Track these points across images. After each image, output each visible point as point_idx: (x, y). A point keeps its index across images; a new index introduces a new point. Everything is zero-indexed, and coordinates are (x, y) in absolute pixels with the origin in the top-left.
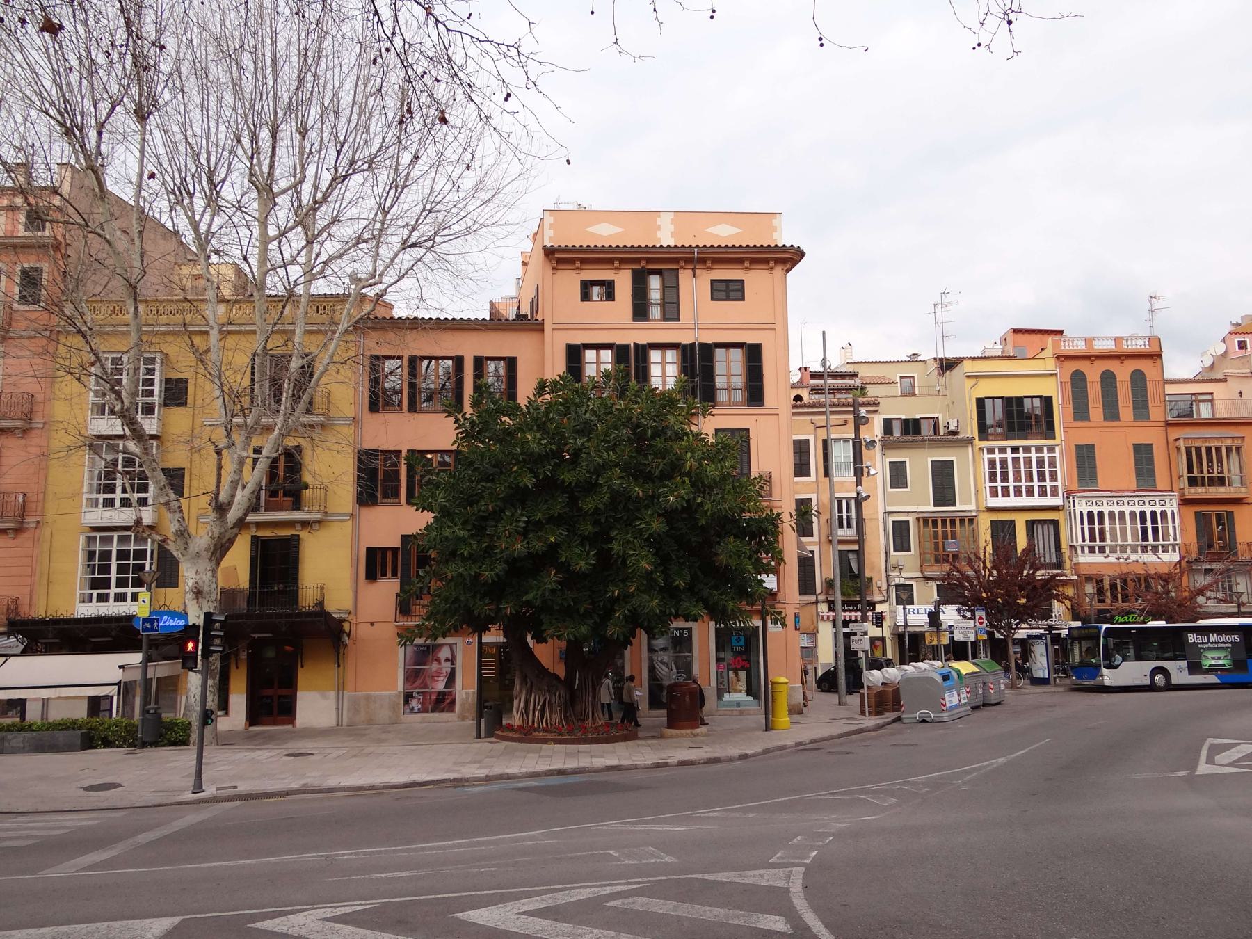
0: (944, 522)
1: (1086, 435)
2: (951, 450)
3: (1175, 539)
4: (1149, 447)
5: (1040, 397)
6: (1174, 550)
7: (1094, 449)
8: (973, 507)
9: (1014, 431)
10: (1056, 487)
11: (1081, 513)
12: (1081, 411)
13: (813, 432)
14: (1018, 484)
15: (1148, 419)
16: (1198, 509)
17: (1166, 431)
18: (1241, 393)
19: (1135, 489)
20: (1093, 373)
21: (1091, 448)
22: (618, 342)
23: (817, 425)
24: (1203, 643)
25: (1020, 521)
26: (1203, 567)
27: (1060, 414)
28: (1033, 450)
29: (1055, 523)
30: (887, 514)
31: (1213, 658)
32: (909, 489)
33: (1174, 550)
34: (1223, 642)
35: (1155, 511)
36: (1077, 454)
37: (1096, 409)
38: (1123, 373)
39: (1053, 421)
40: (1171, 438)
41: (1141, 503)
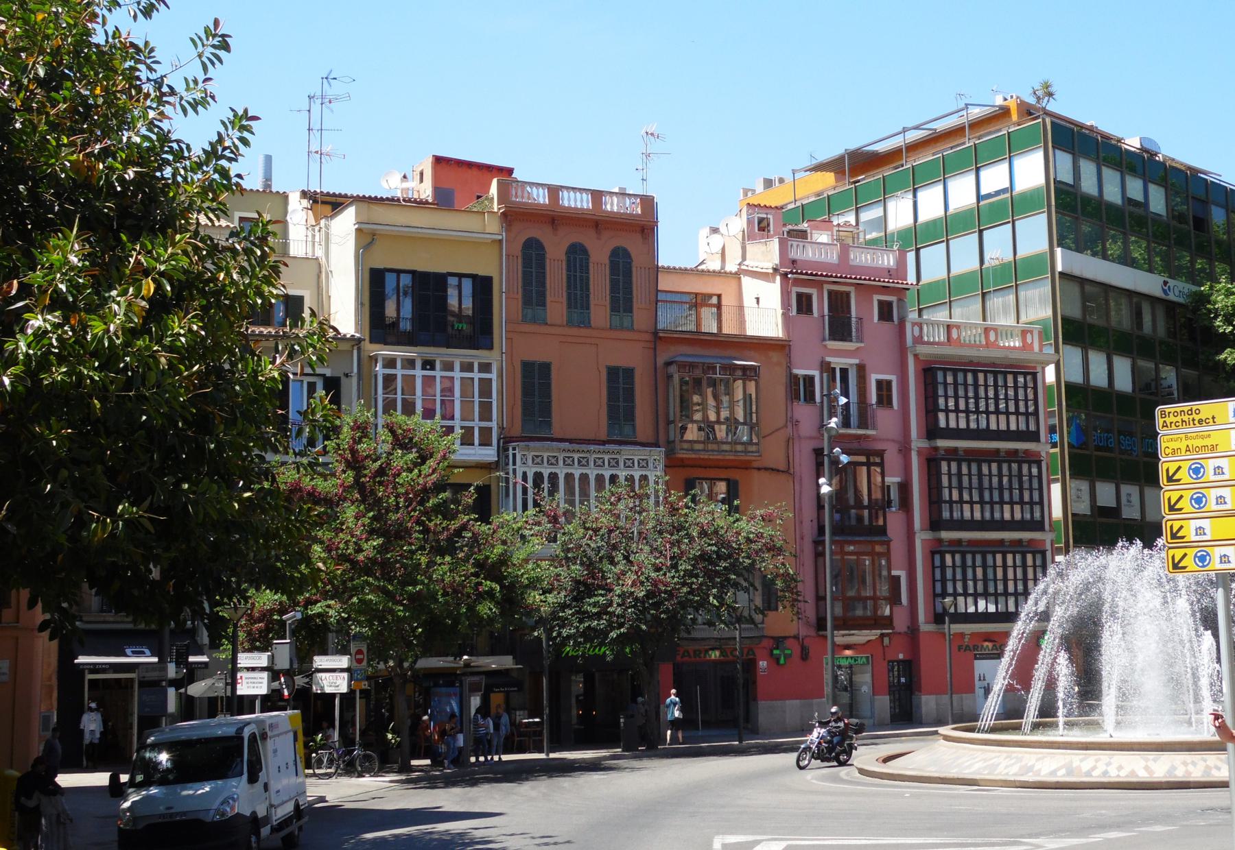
4: (629, 373)
5: (413, 273)
11: (525, 474)
14: (485, 424)
17: (655, 349)
18: (758, 299)
21: (545, 368)
22: (481, 273)
27: (503, 307)
35: (602, 475)
37: (556, 304)
38: (599, 254)
39: (491, 319)
40: (660, 361)
41: (613, 463)
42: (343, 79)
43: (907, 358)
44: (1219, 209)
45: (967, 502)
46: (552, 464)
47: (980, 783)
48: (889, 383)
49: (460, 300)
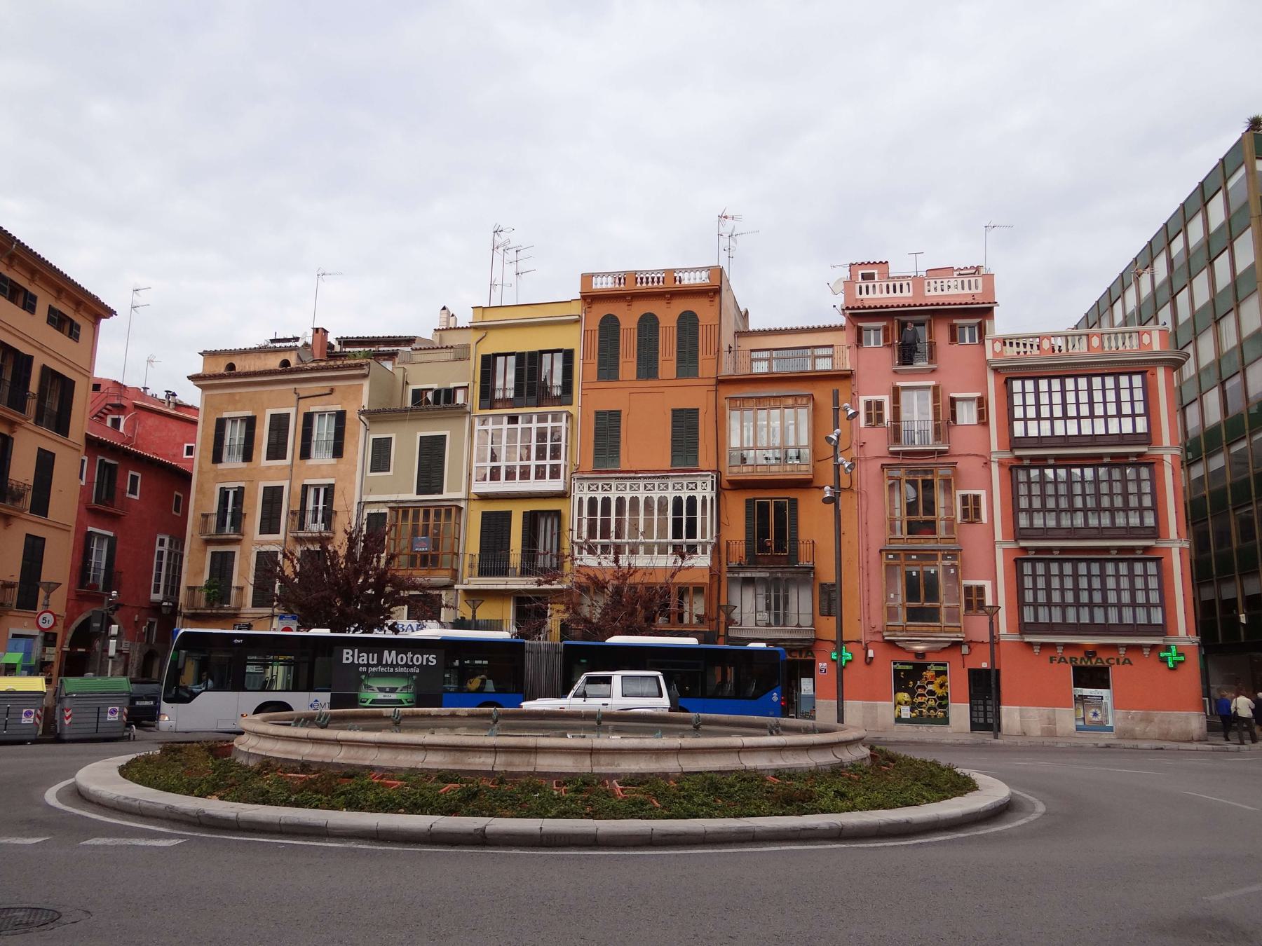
0: (427, 513)
1: (610, 398)
2: (384, 426)
3: (704, 536)
4: (694, 413)
6: (704, 552)
7: (620, 416)
8: (462, 495)
9: (522, 395)
10: (558, 466)
12: (608, 367)
13: (295, 404)
15: (696, 375)
16: (751, 495)
19: (670, 468)
20: (629, 318)
21: (615, 415)
23: (301, 396)
24: (368, 665)
25: (518, 512)
26: (741, 575)
28: (535, 418)
29: (557, 514)
30: (362, 504)
31: (382, 690)
32: (391, 473)
33: (704, 552)
34: (406, 665)
35: (595, 498)
36: (596, 423)
37: (628, 365)
38: (668, 316)
41: (662, 487)
42: (507, 230)
43: (925, 315)
44: (1223, 460)
45: (1113, 605)
46: (605, 490)
47: (1111, 746)
48: (879, 405)
49: (553, 371)
